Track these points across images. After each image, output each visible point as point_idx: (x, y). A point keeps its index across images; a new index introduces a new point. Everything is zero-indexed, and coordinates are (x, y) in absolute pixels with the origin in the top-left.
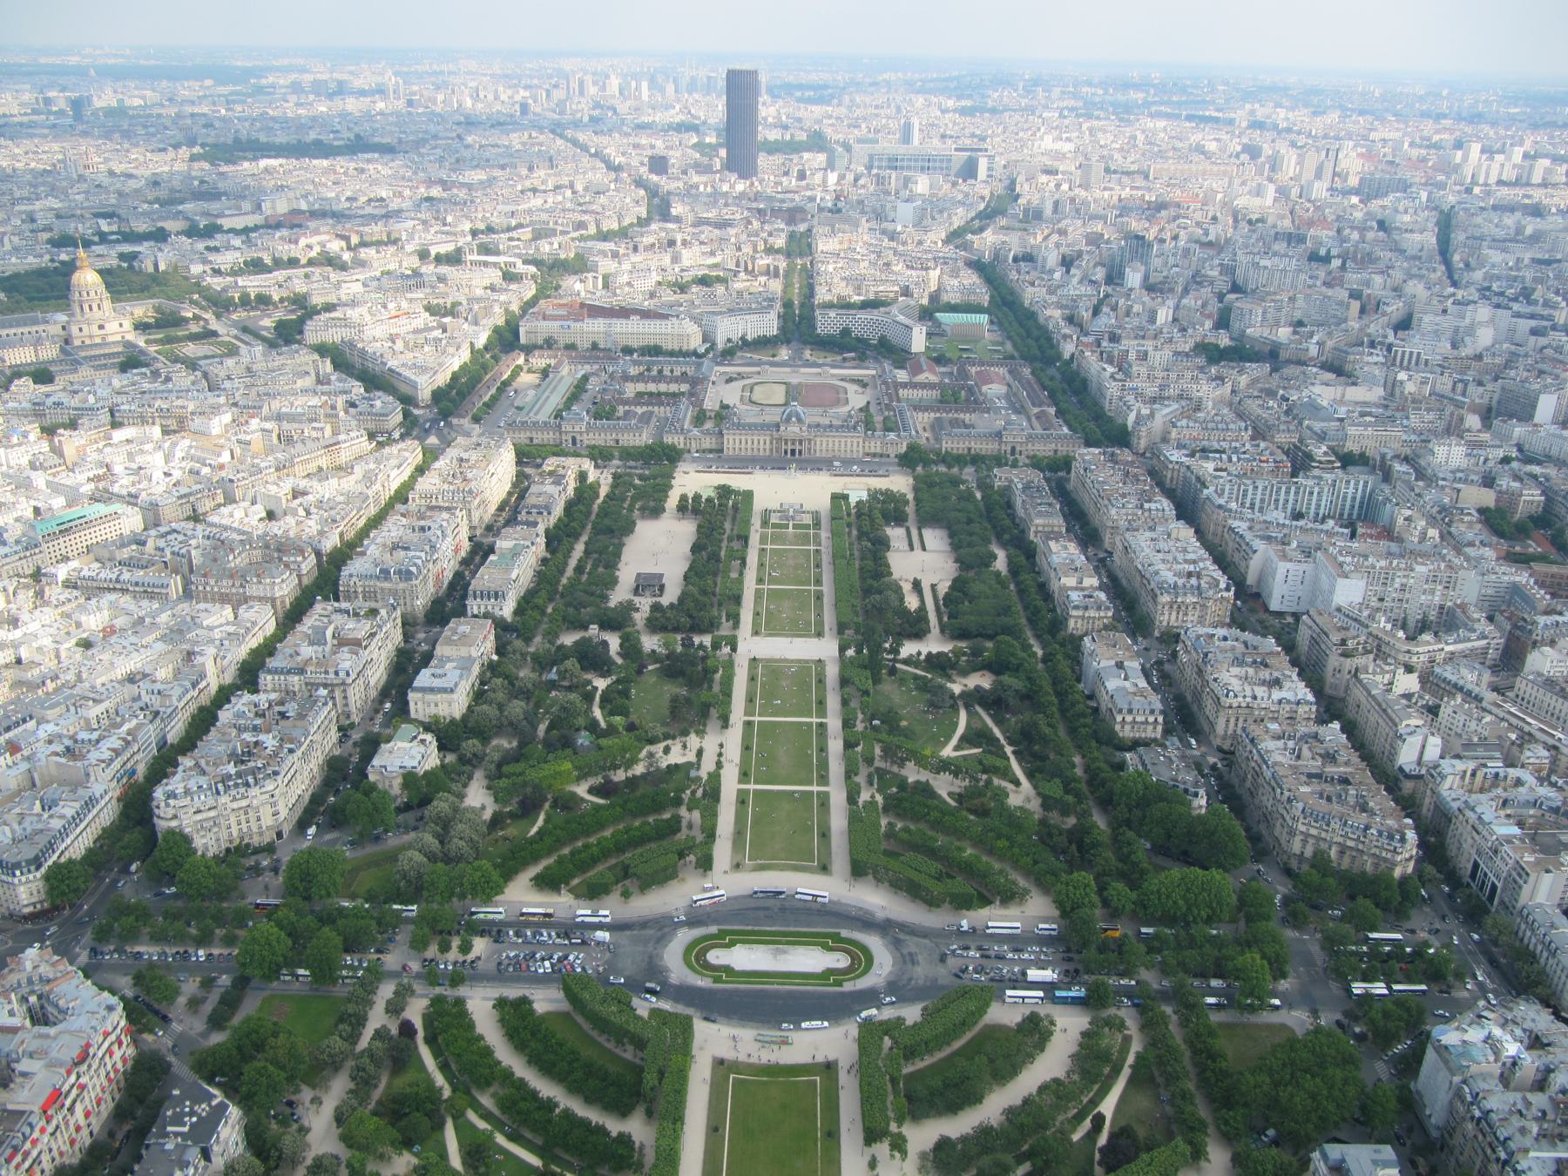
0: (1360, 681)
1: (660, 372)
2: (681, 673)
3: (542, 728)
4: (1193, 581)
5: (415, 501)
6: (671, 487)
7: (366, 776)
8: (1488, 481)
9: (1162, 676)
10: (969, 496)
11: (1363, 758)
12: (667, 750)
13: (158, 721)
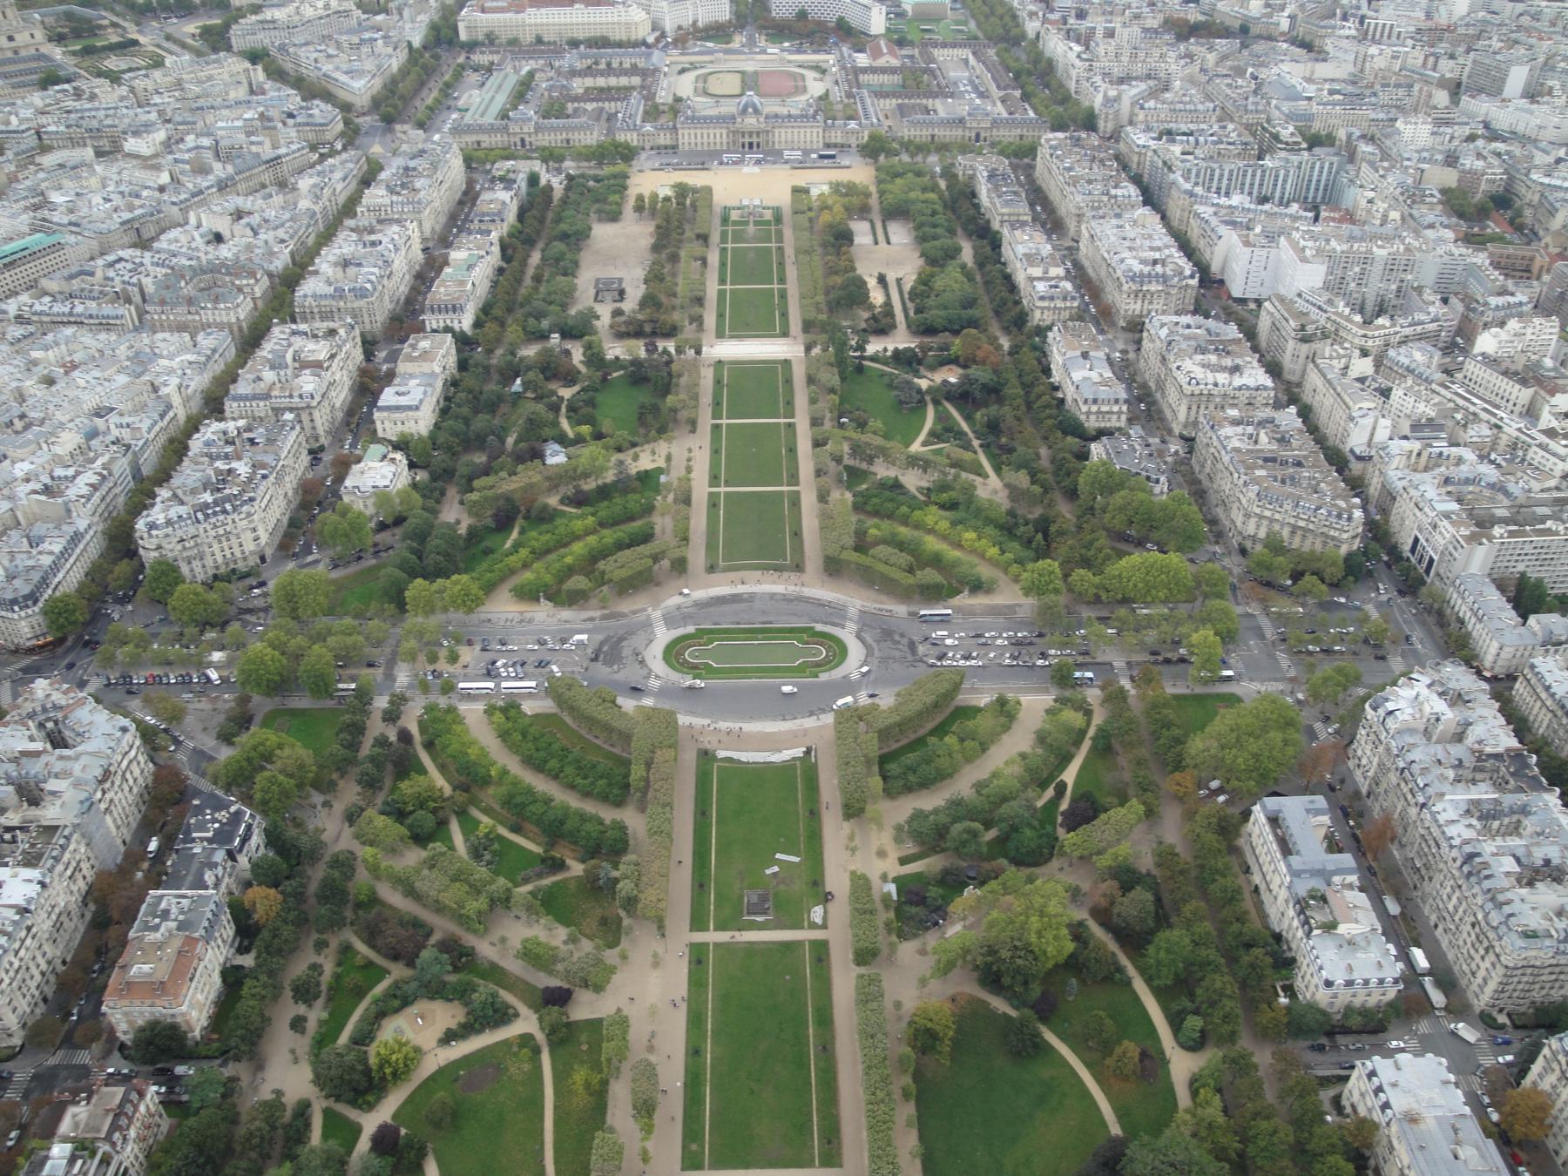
0: (1317, 366)
1: (609, 64)
2: (646, 380)
3: (510, 441)
4: (1159, 268)
5: (363, 217)
8: (1451, 160)
9: (1125, 371)
10: (934, 188)
11: (1317, 441)
12: (636, 458)
13: (129, 455)
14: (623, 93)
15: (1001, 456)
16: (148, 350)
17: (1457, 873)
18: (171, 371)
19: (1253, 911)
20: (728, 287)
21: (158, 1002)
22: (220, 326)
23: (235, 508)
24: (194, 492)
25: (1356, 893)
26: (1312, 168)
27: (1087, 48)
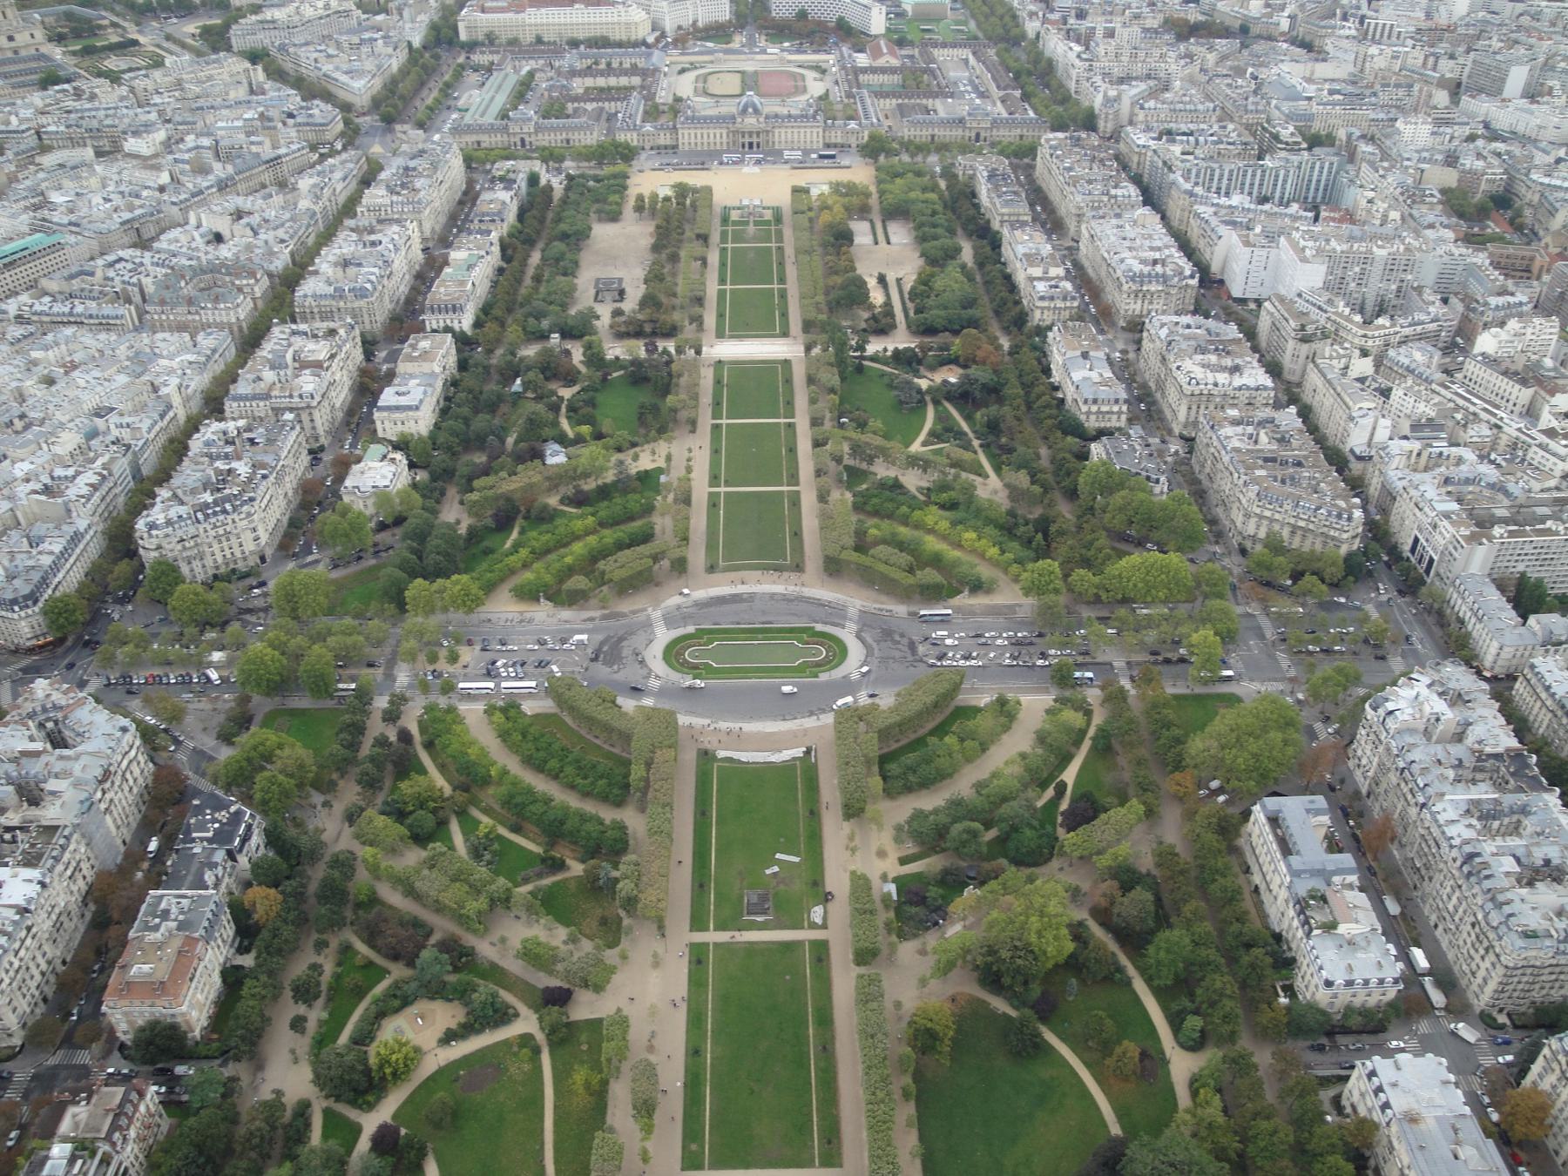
0: (1317, 366)
1: (609, 64)
2: (646, 380)
3: (510, 441)
4: (1159, 268)
5: (364, 217)
8: (1451, 160)
9: (1125, 371)
10: (934, 188)
11: (1317, 441)
12: (636, 458)
13: (129, 454)
14: (623, 93)
15: (1001, 456)
18: (171, 372)
19: (1253, 911)
20: (728, 287)
21: (158, 1002)
22: (220, 326)
23: (235, 509)
24: (194, 492)
25: (1356, 893)
26: (1313, 168)
27: (1087, 48)
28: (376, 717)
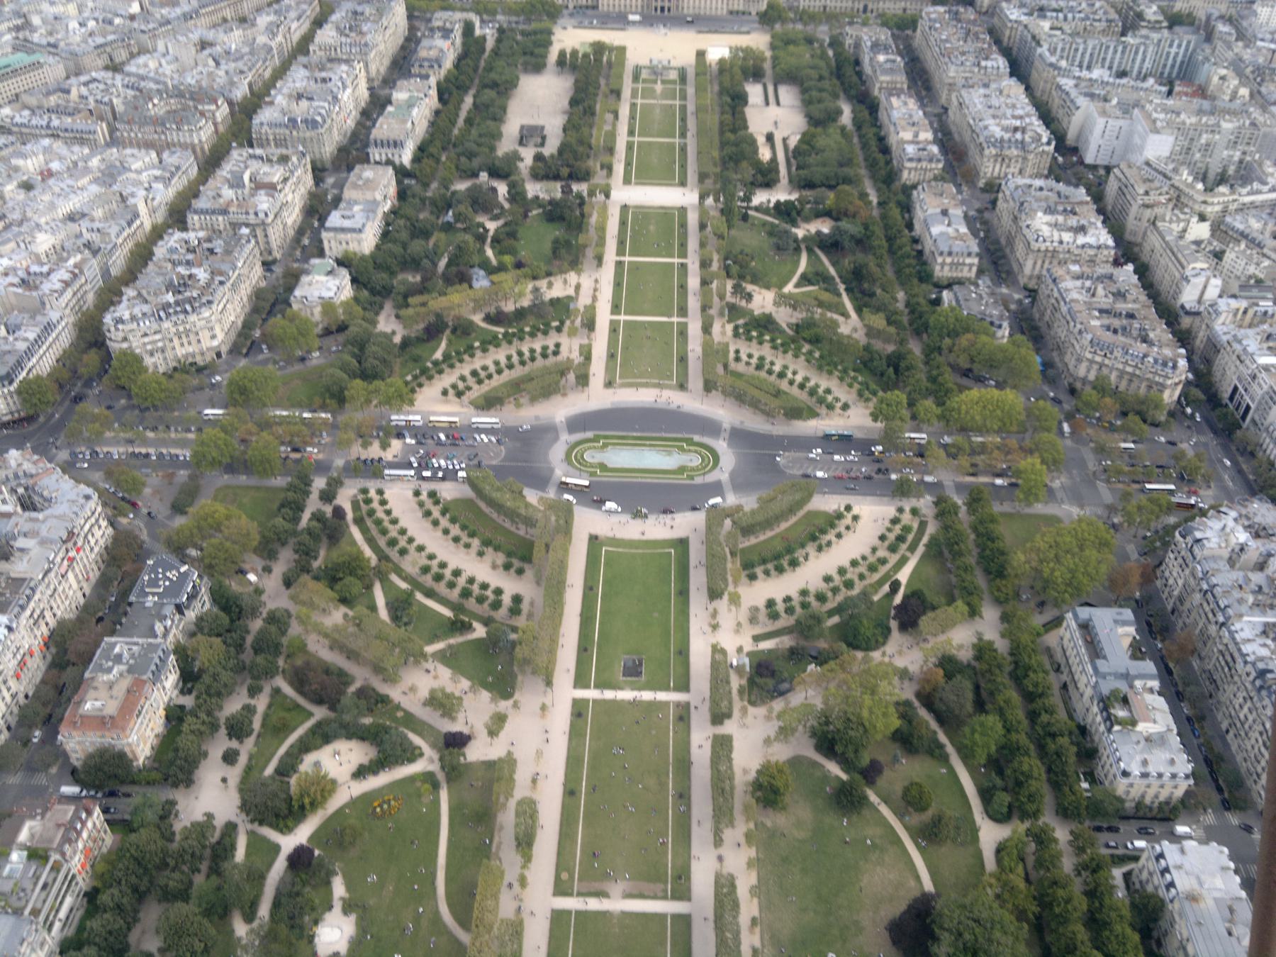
2: (562, 218)
3: (443, 263)
4: (1019, 136)
6: (550, 43)
7: (290, 306)
10: (823, 55)
11: (1149, 296)
12: (550, 285)
15: (864, 300)
16: (118, 164)
17: (1249, 687)
19: (1061, 705)
21: (107, 734)
22: (184, 146)
23: (194, 310)
28: (314, 496)
